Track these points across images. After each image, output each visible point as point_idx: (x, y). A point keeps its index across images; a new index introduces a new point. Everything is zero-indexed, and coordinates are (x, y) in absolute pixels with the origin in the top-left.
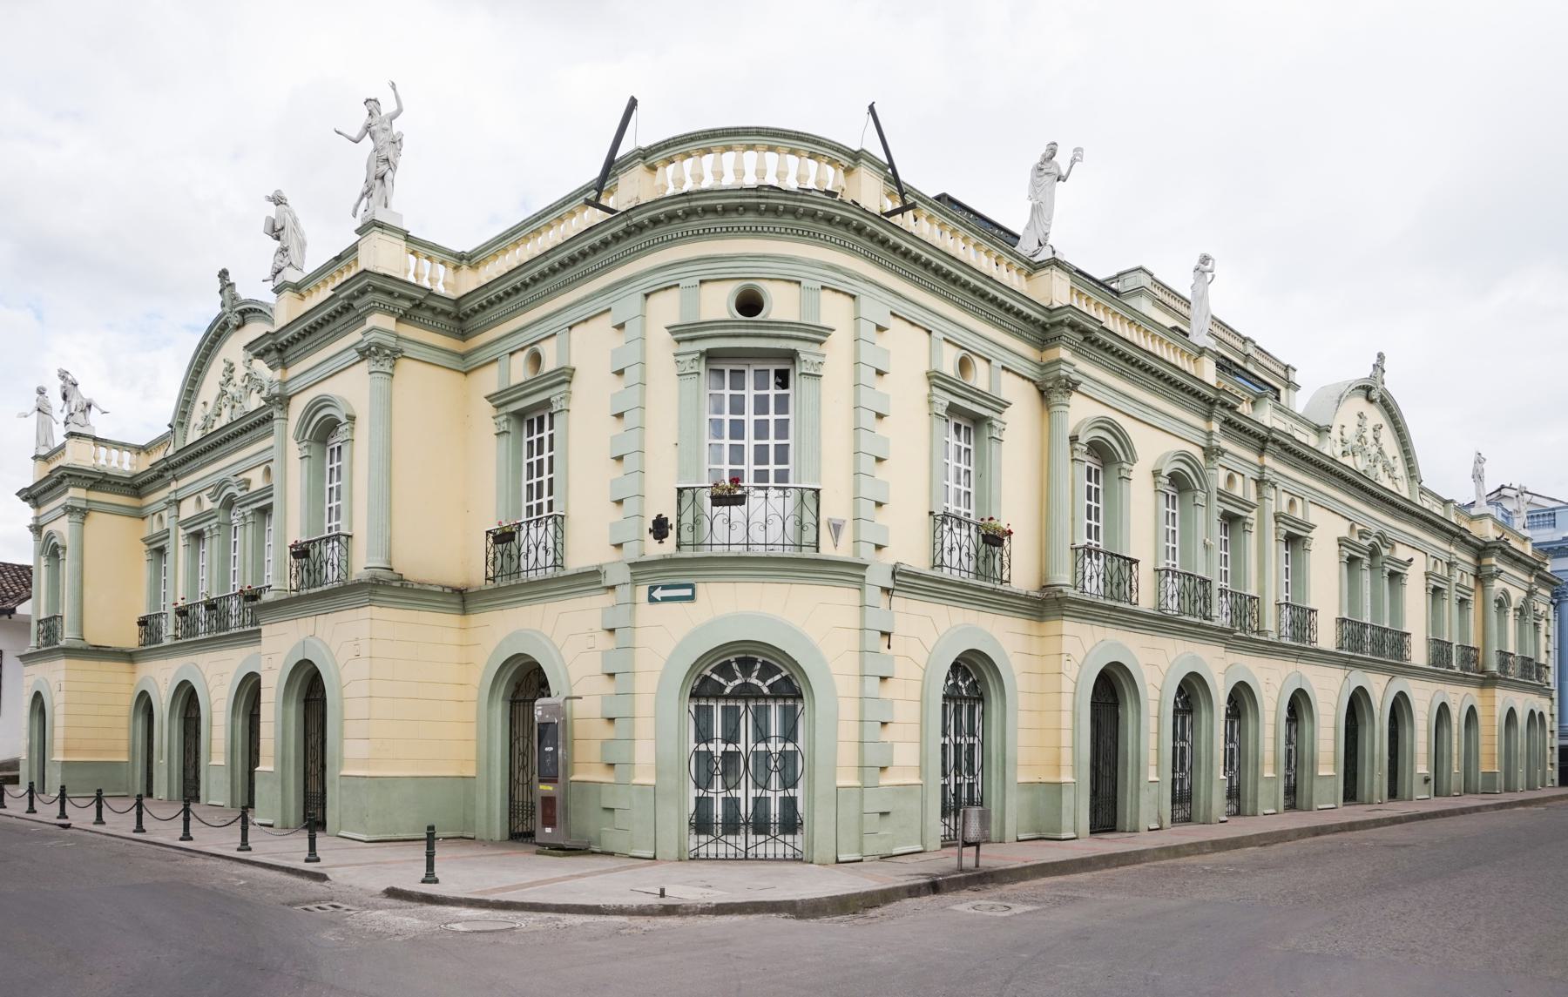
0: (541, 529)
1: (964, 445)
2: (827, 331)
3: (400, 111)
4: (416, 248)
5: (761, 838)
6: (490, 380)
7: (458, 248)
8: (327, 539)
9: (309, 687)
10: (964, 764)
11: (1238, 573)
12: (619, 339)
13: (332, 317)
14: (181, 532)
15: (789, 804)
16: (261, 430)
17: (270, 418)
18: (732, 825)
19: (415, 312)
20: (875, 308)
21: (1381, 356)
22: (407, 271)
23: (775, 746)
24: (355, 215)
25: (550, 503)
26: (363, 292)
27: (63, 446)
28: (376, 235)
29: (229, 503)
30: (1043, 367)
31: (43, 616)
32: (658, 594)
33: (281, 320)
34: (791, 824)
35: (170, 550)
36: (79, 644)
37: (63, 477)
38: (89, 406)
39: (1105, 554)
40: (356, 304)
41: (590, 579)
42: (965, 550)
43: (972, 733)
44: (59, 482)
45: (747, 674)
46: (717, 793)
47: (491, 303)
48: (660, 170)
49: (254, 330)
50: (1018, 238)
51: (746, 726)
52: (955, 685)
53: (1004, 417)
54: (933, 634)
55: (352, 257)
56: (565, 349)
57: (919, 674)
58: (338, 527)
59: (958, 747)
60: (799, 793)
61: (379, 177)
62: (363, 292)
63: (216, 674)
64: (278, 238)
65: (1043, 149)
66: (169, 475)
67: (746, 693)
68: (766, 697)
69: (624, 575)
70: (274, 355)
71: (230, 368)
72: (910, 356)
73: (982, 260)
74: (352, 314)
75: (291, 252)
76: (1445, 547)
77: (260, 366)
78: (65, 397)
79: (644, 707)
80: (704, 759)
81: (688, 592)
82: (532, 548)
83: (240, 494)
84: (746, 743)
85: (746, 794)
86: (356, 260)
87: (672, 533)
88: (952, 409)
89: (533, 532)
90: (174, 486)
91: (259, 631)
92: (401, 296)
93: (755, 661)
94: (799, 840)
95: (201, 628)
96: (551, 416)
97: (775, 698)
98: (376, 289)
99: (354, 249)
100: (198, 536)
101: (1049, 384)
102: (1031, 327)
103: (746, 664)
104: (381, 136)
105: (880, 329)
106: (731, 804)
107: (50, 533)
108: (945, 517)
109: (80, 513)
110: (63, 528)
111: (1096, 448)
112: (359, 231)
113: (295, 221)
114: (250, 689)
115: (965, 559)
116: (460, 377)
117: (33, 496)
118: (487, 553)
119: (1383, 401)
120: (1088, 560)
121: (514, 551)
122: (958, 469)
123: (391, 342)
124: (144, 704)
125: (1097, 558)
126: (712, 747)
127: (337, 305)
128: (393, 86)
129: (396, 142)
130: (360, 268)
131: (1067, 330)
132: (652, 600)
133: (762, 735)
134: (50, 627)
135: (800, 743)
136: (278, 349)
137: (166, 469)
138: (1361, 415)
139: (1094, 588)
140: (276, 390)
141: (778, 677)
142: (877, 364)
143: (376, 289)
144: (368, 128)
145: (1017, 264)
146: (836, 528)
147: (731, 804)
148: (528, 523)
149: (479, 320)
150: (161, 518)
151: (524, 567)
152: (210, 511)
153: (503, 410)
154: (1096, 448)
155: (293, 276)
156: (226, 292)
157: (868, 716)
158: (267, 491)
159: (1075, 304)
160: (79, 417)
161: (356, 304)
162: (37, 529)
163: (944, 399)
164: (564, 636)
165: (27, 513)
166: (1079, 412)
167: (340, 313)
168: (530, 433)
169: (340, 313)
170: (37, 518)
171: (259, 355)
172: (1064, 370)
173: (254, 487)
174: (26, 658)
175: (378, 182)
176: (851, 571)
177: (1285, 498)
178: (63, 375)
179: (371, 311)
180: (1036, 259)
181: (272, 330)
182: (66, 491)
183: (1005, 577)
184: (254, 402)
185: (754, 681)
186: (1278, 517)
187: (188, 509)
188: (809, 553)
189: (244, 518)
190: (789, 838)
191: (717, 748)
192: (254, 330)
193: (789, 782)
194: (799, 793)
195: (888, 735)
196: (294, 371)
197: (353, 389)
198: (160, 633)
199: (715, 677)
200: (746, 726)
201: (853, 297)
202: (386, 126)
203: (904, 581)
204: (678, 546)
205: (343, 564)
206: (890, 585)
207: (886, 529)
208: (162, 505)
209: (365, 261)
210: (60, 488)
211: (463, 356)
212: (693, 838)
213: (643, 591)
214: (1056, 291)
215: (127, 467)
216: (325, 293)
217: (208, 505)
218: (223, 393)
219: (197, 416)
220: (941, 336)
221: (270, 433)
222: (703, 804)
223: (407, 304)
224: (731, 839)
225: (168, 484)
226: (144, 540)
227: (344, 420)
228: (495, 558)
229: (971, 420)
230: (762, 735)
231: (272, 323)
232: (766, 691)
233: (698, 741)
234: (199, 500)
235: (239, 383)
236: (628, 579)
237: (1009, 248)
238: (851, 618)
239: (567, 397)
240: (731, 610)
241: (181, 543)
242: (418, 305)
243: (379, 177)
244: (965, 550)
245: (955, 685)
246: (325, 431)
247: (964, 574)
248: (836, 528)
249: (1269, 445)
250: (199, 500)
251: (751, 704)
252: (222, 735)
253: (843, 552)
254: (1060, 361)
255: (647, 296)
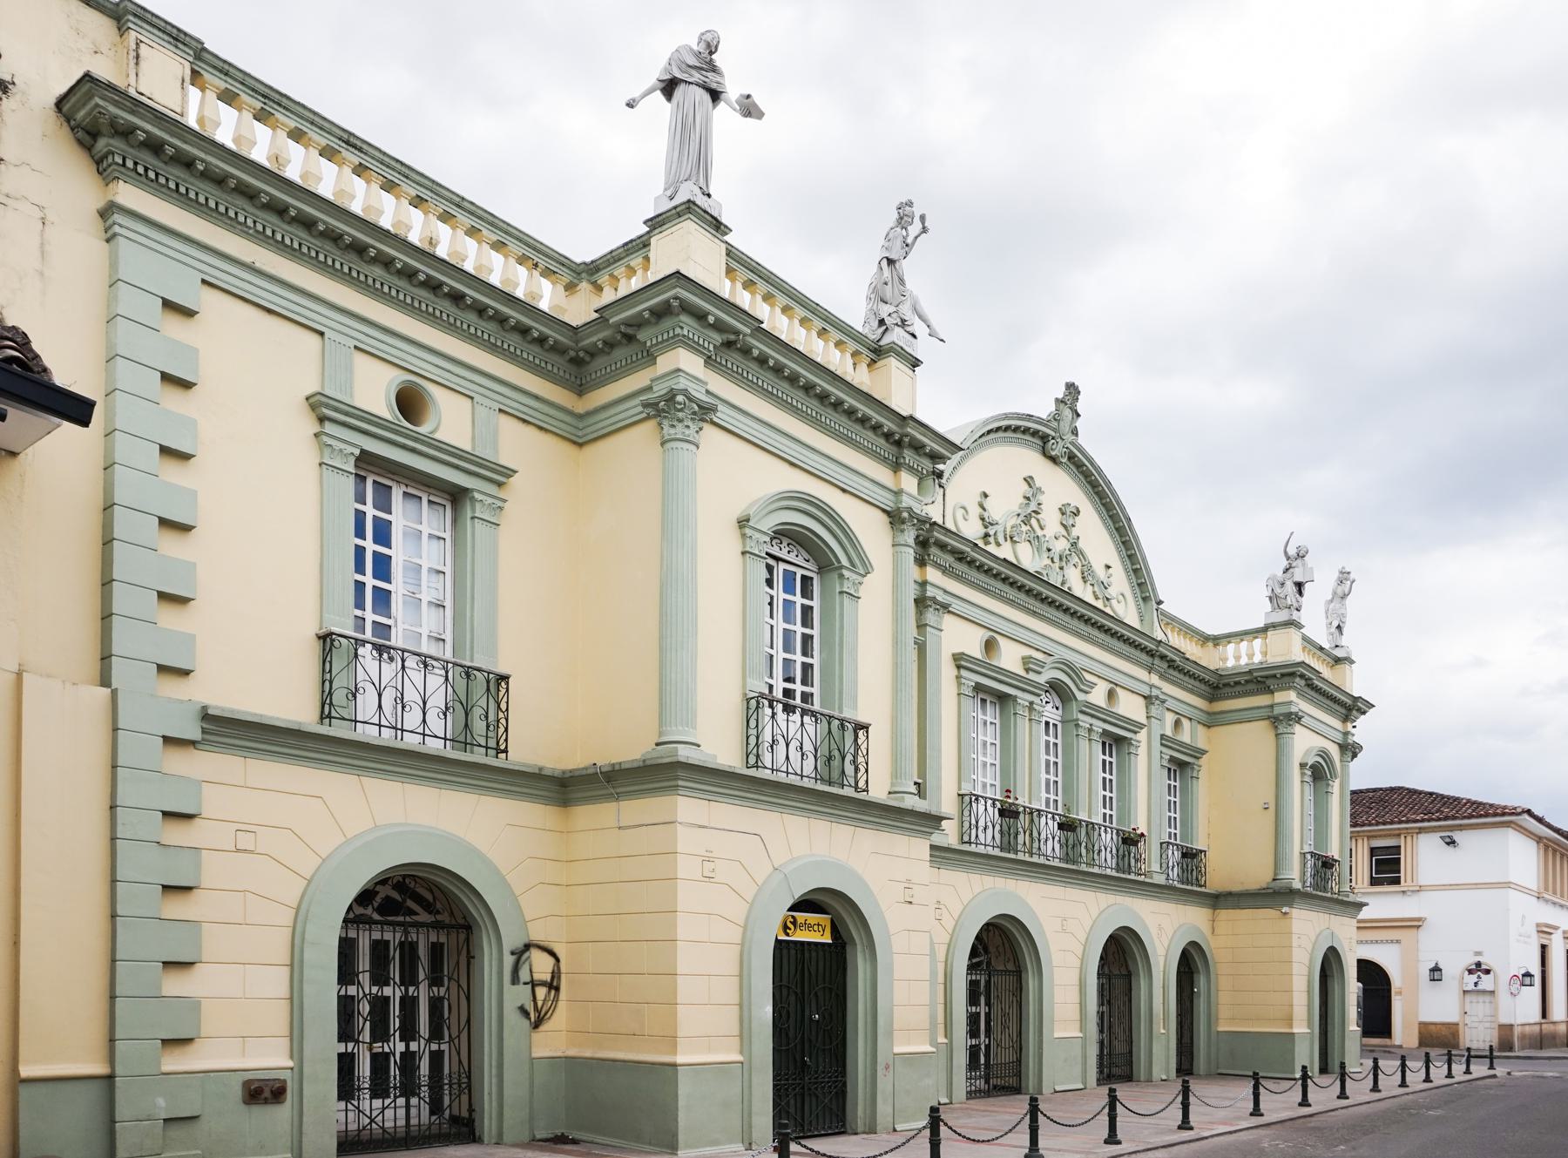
11: (1126, 809)
21: (1073, 390)
53: (1201, 762)
76: (1141, 674)
119: (1071, 457)
138: (1029, 480)
177: (1170, 718)
186: (960, 660)
247: (387, 733)
249: (934, 550)
252: (1073, 1012)
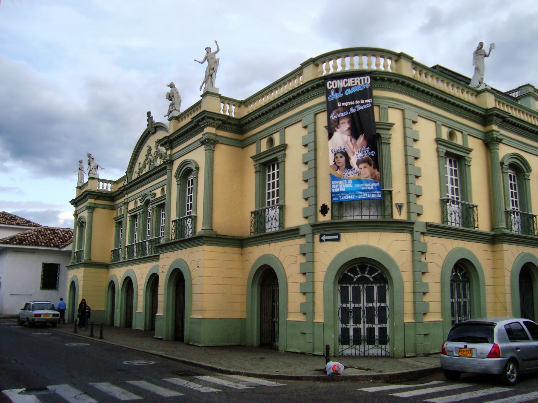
0: (274, 211)
1: (453, 168)
2: (392, 125)
3: (218, 50)
4: (223, 100)
5: (371, 346)
6: (252, 150)
7: (240, 99)
8: (187, 218)
9: (178, 278)
10: (462, 311)
12: (305, 132)
13: (191, 129)
14: (129, 215)
15: (383, 331)
16: (162, 173)
17: (165, 168)
18: (357, 341)
19: (223, 125)
20: (411, 114)
22: (220, 109)
23: (376, 305)
24: (200, 90)
25: (277, 200)
26: (203, 119)
27: (87, 182)
28: (208, 97)
29: (147, 203)
30: (486, 133)
31: (76, 250)
32: (324, 238)
33: (171, 131)
34: (384, 339)
35: (124, 223)
36: (89, 262)
37: (87, 195)
38: (97, 167)
39: (521, 213)
40: (200, 124)
41: (294, 233)
42: (457, 214)
43: (465, 297)
44: (85, 197)
45: (363, 272)
46: (351, 326)
47: (253, 120)
48: (320, 66)
49: (160, 135)
50: (470, 80)
51: (363, 296)
52: (456, 275)
53: (470, 156)
54: (441, 252)
55: (199, 105)
56: (283, 137)
57: (439, 270)
58: (190, 212)
59: (459, 303)
60: (387, 325)
61: (211, 74)
62: (203, 119)
63: (141, 273)
64: (171, 100)
65: (477, 45)
66: (125, 192)
67: (363, 280)
68: (372, 283)
69: (309, 231)
70: (168, 144)
71: (150, 149)
72: (426, 132)
73: (455, 92)
74: (199, 128)
75: (175, 105)
77: (163, 149)
78: (89, 164)
79: (319, 287)
80: (345, 311)
81: (337, 237)
82: (270, 219)
83: (152, 199)
84: (363, 304)
85: (363, 327)
86: (200, 107)
87: (329, 212)
88: (448, 154)
89: (270, 212)
90: (126, 197)
91: (159, 255)
92: (218, 120)
93: (366, 267)
94: (388, 347)
95: (135, 254)
96: (278, 164)
97: (376, 283)
98: (208, 118)
99: (200, 103)
100: (134, 217)
101: (489, 140)
102: (478, 117)
103: (363, 268)
104: (211, 60)
105: (414, 122)
106: (357, 331)
107: (81, 217)
108: (448, 201)
109: (91, 208)
110: (85, 214)
111: (512, 166)
112: (201, 96)
113: (177, 93)
114: (154, 280)
115: (457, 218)
116: (241, 149)
117: (75, 202)
118: (251, 222)
120: (513, 216)
121: (263, 221)
122: (452, 179)
123: (214, 137)
124: (112, 285)
125: (517, 215)
126: (348, 305)
127: (193, 124)
128: (216, 42)
129: (217, 62)
130: (202, 109)
131: (495, 118)
132: (321, 241)
133: (370, 299)
134: (79, 254)
135: (388, 303)
136: (169, 142)
137: (124, 190)
139: (516, 229)
140: (168, 158)
141: (376, 274)
142: (416, 138)
143: (208, 118)
144: (206, 58)
145: (471, 92)
146: (400, 207)
147: (357, 331)
148: (268, 208)
149: (249, 126)
150: (121, 209)
151: (267, 228)
152: (141, 206)
153: (258, 162)
154: (512, 166)
155: (175, 114)
156: (150, 120)
157: (417, 290)
158: (163, 197)
159: (498, 107)
160: (94, 171)
161: (200, 124)
162: (76, 215)
163: (443, 149)
164: (285, 255)
165: (73, 209)
166: (504, 151)
167: (195, 127)
168: (269, 171)
169: (195, 127)
170: (76, 211)
171: (162, 145)
172: (495, 135)
173: (157, 196)
174: (70, 267)
175: (210, 77)
176: (406, 226)
178: (89, 156)
179: (206, 126)
180: (479, 89)
181: (168, 135)
182: (87, 200)
183: (476, 225)
184: (159, 162)
185: (367, 276)
187: (131, 206)
188: (388, 219)
189: (153, 209)
190: (383, 346)
191: (351, 306)
192: (160, 135)
193: (383, 320)
194: (387, 325)
195: (426, 299)
196: (175, 150)
197: (198, 156)
198: (118, 256)
199: (349, 274)
200: (363, 296)
201: (402, 110)
202: (213, 56)
203: (432, 230)
204: (332, 217)
205: (193, 228)
206: (425, 230)
207: (421, 206)
208: (122, 204)
209: (204, 107)
210: (85, 200)
211: (242, 141)
212: (341, 346)
213: (317, 237)
214: (490, 102)
215: (109, 190)
216: (188, 120)
217: (139, 204)
218: (147, 159)
219: (136, 169)
220: (440, 123)
221: (165, 174)
222: (345, 331)
223: (220, 122)
224: (357, 347)
225: (124, 196)
226: (114, 219)
227: (194, 169)
228: (255, 224)
229: (456, 158)
230: (370, 299)
231: (167, 132)
232: (371, 279)
233: (342, 302)
234: (136, 202)
235: (153, 155)
236: (311, 232)
237: (466, 85)
238: (408, 245)
239: (285, 156)
240: (354, 242)
241: (128, 219)
242: (224, 122)
243: (211, 74)
244: (457, 214)
245: (456, 275)
246: (187, 173)
248: (400, 207)
250: (136, 202)
251: (365, 286)
253: (402, 216)
254: (493, 131)
255: (316, 114)
